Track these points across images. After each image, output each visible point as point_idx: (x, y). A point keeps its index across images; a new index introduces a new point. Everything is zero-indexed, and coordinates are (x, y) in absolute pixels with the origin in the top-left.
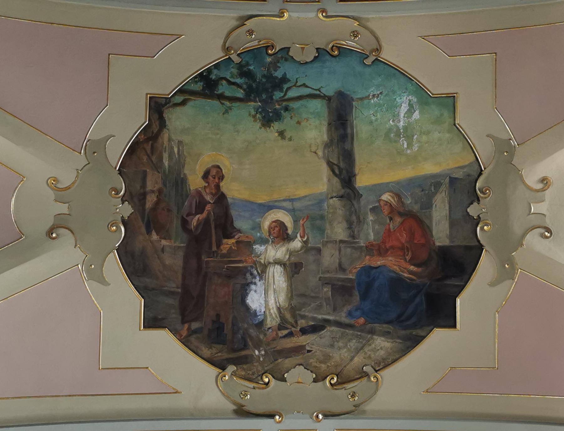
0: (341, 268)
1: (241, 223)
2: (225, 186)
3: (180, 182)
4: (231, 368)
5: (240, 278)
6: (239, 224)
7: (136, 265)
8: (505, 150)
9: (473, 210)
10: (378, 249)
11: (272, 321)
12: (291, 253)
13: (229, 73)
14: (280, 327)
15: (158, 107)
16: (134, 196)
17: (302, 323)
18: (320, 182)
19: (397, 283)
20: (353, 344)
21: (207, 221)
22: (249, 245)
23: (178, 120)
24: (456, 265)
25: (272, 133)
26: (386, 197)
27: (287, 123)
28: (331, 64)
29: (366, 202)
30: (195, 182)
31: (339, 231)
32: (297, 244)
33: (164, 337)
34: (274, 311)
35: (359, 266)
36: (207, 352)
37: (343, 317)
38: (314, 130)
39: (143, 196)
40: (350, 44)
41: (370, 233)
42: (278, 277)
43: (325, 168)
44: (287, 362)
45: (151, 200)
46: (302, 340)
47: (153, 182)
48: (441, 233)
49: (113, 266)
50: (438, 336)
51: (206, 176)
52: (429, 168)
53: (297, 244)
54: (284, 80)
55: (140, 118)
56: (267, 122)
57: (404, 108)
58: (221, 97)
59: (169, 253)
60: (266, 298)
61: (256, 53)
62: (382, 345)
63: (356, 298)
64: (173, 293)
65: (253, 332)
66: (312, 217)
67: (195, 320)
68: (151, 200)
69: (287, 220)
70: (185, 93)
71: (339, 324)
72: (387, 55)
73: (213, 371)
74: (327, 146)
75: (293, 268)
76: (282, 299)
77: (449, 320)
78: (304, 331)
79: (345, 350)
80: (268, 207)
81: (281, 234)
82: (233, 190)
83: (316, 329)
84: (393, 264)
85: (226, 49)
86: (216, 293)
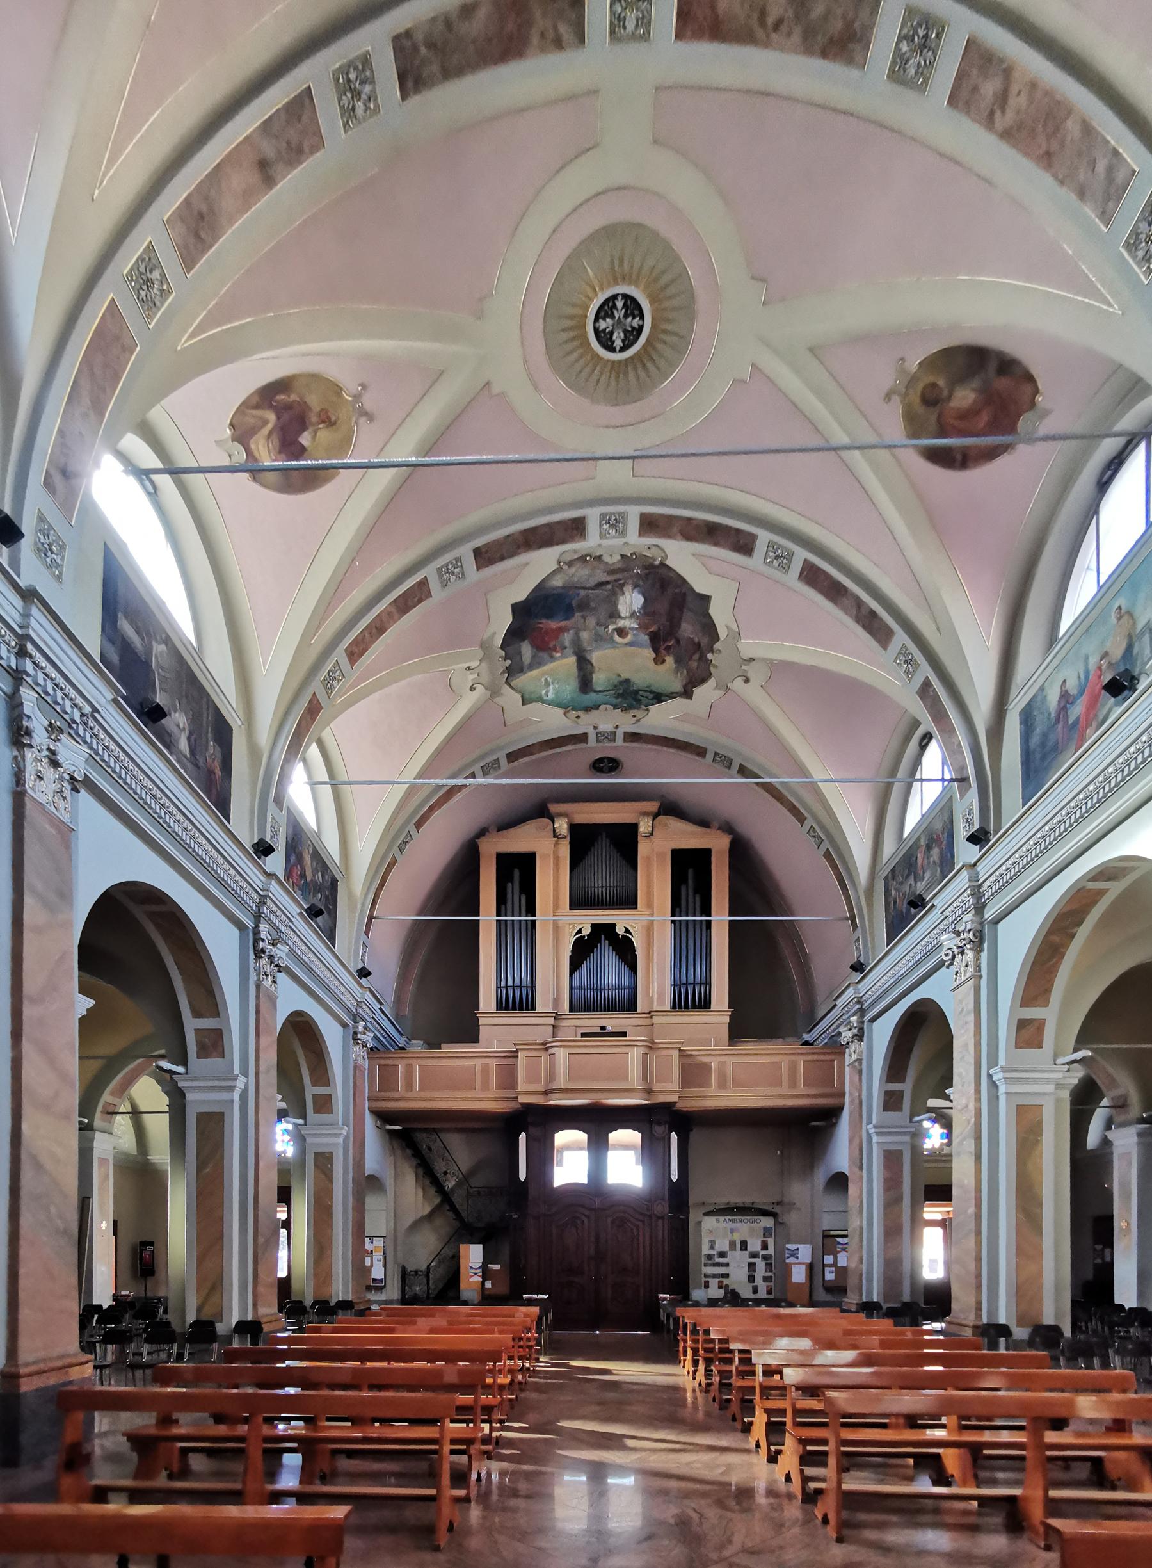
0: (584, 618)
1: (645, 638)
2: (654, 655)
3: (678, 661)
4: (657, 563)
5: (648, 612)
6: (647, 637)
7: (710, 629)
8: (494, 692)
9: (508, 662)
10: (562, 630)
11: (628, 589)
12: (615, 623)
13: (644, 701)
14: (623, 585)
15: (687, 693)
16: (703, 659)
17: (609, 587)
18: (596, 657)
19: (549, 616)
20: (576, 579)
21: (665, 641)
22: (641, 627)
23: (677, 686)
24: (515, 634)
25: (624, 676)
26: (558, 655)
27: (616, 681)
28: (591, 704)
29: (569, 651)
30: (670, 660)
31: (585, 635)
32: (611, 628)
33: (699, 589)
34: (627, 593)
35: (573, 620)
36: (671, 574)
37: (583, 593)
38: (600, 679)
39: (700, 659)
40: (580, 713)
41: (567, 638)
42: (623, 610)
43: (594, 662)
44: (620, 565)
45: (696, 657)
46: (609, 578)
47: (694, 664)
48: (526, 650)
49: (722, 633)
50: (521, 595)
51: (664, 661)
52: (534, 673)
53: (611, 628)
54: (617, 698)
55: (698, 691)
56: (627, 681)
57: (550, 694)
58: (651, 692)
59: (688, 629)
60: (631, 601)
61: (631, 707)
62: (558, 582)
63: (574, 603)
64: (690, 610)
65: (641, 583)
66: (600, 639)
67: (676, 594)
68: (696, 657)
69: (616, 638)
70: (672, 696)
71: (585, 588)
72: (561, 711)
73: (668, 562)
74: (591, 673)
75: (614, 615)
76: (621, 599)
77: (515, 608)
78: (608, 583)
79: (799, 1275)
80: (631, 644)
81: (621, 632)
82: (649, 653)
83: (600, 585)
84: (553, 624)
85: (648, 710)
86: (662, 607)
